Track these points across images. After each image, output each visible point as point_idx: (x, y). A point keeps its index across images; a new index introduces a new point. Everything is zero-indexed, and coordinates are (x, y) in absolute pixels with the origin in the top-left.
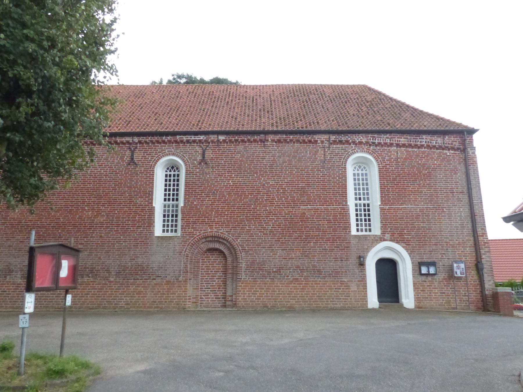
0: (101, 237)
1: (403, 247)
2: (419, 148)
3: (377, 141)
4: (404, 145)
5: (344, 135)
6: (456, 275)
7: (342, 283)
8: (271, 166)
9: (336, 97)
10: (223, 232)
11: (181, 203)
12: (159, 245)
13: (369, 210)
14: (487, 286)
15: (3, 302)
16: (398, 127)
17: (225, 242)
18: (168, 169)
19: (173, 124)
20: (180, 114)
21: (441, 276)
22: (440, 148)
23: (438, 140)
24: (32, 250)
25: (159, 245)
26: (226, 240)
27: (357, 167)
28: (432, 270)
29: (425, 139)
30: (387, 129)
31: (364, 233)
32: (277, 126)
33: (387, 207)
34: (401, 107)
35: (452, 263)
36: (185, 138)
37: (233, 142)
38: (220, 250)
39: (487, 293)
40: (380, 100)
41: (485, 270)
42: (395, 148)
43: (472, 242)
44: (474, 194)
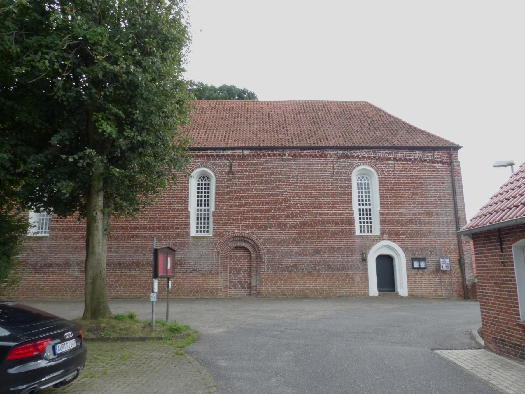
0: (145, 236)
1: (399, 245)
2: (413, 161)
3: (377, 156)
4: (400, 159)
5: (349, 151)
6: (442, 269)
7: (348, 275)
8: (288, 177)
9: (342, 113)
10: (248, 232)
11: (212, 208)
12: (195, 243)
13: (370, 214)
14: (467, 277)
16: (396, 143)
17: (250, 241)
18: (200, 178)
19: (203, 140)
20: (207, 130)
21: (430, 269)
22: (431, 161)
23: (429, 155)
24: (156, 252)
25: (195, 243)
26: (250, 239)
27: (361, 178)
28: (423, 265)
29: (418, 155)
30: (386, 145)
31: (366, 234)
32: (292, 142)
33: (386, 212)
34: (398, 123)
35: (439, 259)
36: (214, 153)
37: (256, 156)
38: (245, 248)
39: (467, 283)
40: (380, 116)
41: (466, 265)
42: (393, 162)
43: (456, 241)
44: (458, 201)
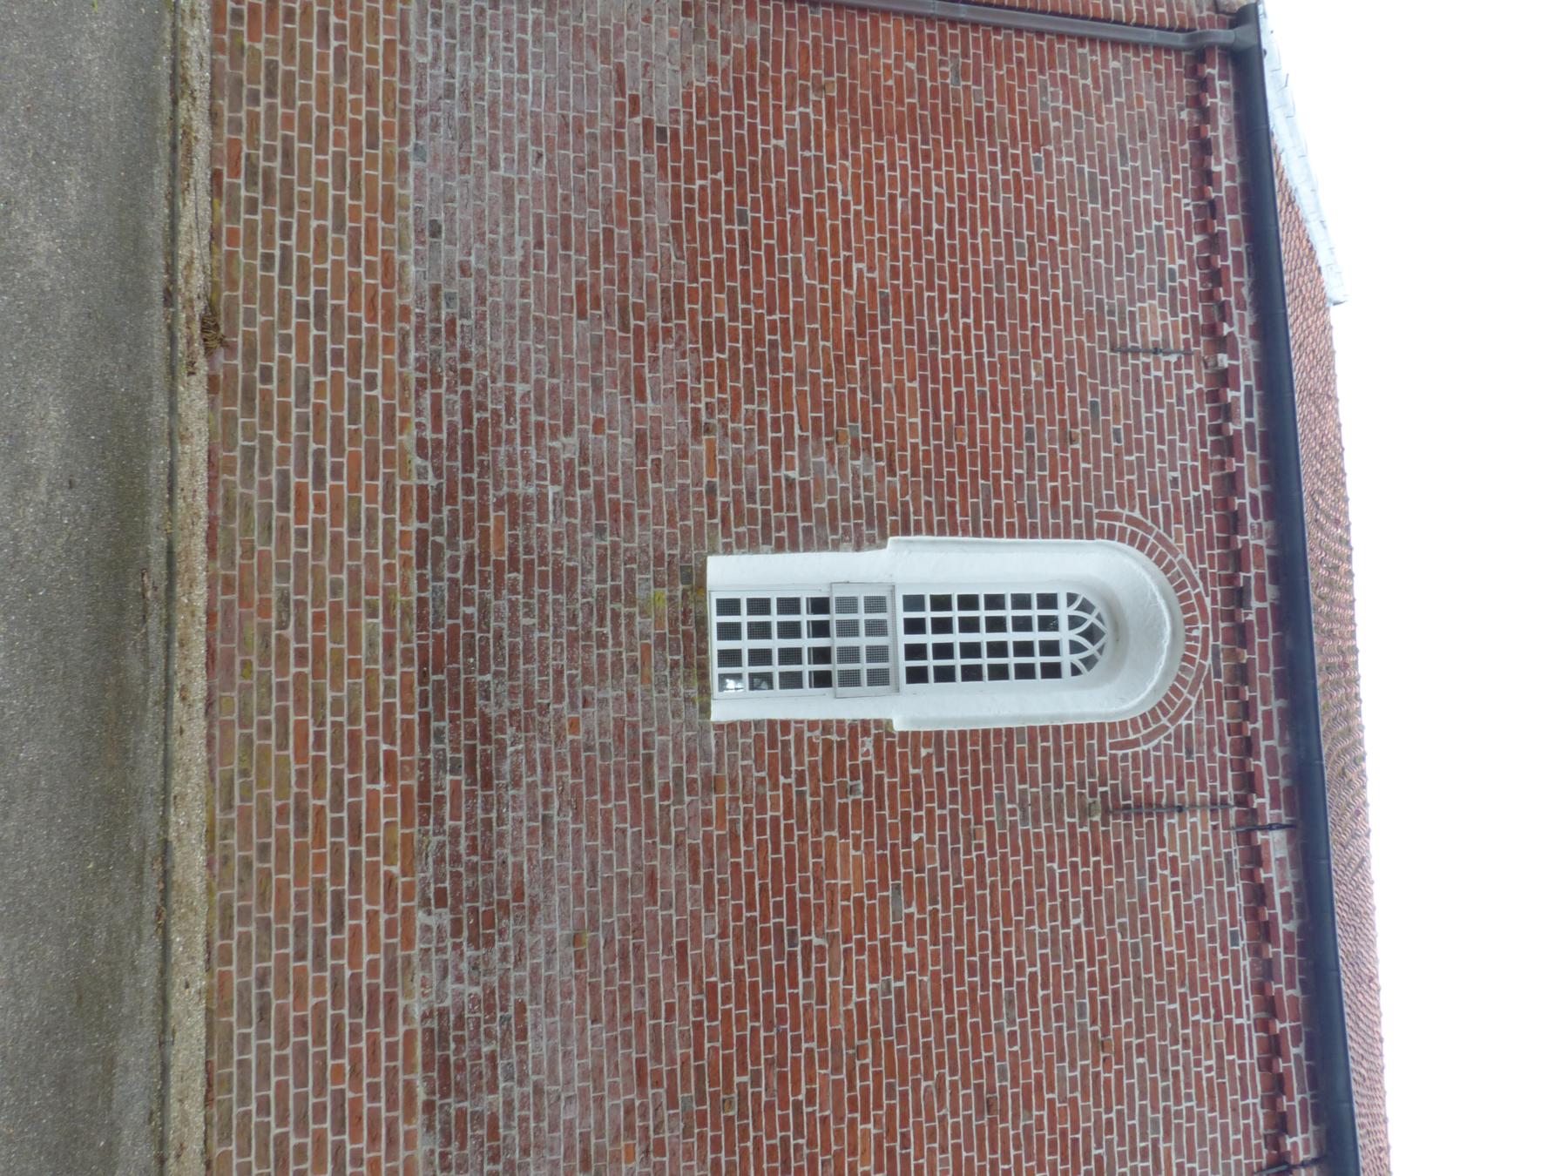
11: (911, 709)
15: (265, 924)
